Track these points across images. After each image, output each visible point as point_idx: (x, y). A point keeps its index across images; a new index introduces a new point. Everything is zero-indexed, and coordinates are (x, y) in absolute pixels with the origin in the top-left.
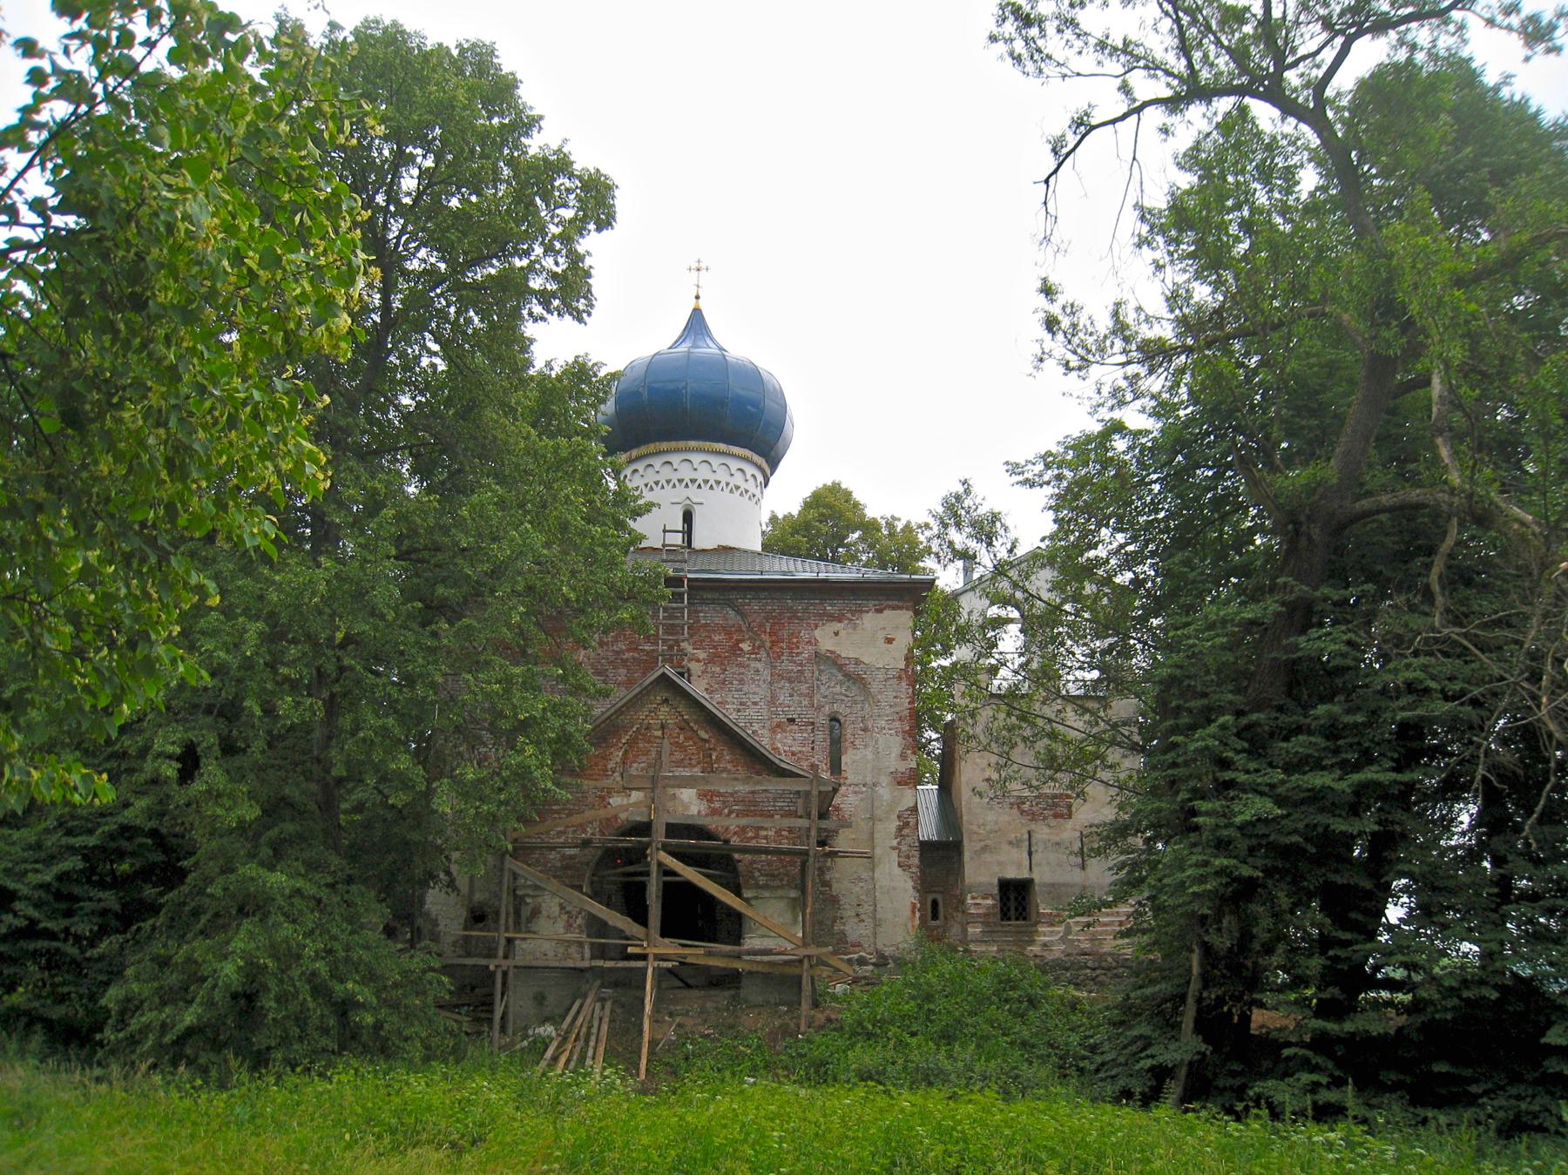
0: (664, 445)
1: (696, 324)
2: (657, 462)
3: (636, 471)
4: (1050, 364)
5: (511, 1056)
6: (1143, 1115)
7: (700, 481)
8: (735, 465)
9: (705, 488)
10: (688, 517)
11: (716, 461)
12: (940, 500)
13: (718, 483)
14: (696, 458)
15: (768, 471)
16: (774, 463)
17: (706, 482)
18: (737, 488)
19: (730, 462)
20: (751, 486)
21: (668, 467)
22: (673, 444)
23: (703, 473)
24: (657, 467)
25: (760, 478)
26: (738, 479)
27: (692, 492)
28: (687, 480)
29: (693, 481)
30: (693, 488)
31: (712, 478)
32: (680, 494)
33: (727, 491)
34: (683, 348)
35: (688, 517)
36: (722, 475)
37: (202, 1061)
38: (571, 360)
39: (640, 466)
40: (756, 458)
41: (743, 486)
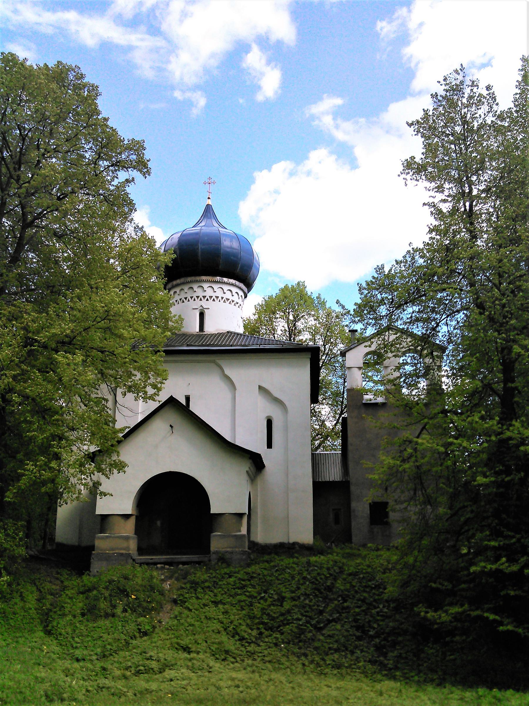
0: (189, 279)
1: (208, 212)
2: (186, 288)
3: (175, 292)
4: (409, 182)
5: (92, 274)
6: (499, 692)
7: (208, 297)
8: (226, 288)
9: (211, 301)
10: (202, 315)
11: (216, 286)
12: (292, 280)
13: (217, 297)
14: (206, 286)
15: (246, 290)
16: (249, 285)
17: (211, 297)
18: (228, 299)
19: (232, 288)
20: (235, 298)
21: (191, 290)
22: (193, 278)
23: (209, 292)
24: (186, 291)
25: (241, 293)
26: (228, 295)
27: (204, 303)
28: (201, 297)
29: (204, 297)
30: (204, 301)
31: (214, 295)
32: (197, 304)
33: (222, 301)
34: (198, 228)
35: (202, 315)
36: (219, 293)
37: (75, 501)
38: (294, 283)
39: (177, 290)
40: (237, 283)
41: (231, 298)
